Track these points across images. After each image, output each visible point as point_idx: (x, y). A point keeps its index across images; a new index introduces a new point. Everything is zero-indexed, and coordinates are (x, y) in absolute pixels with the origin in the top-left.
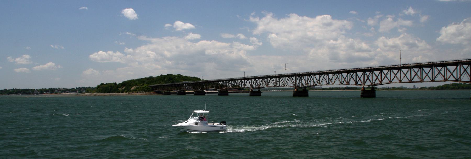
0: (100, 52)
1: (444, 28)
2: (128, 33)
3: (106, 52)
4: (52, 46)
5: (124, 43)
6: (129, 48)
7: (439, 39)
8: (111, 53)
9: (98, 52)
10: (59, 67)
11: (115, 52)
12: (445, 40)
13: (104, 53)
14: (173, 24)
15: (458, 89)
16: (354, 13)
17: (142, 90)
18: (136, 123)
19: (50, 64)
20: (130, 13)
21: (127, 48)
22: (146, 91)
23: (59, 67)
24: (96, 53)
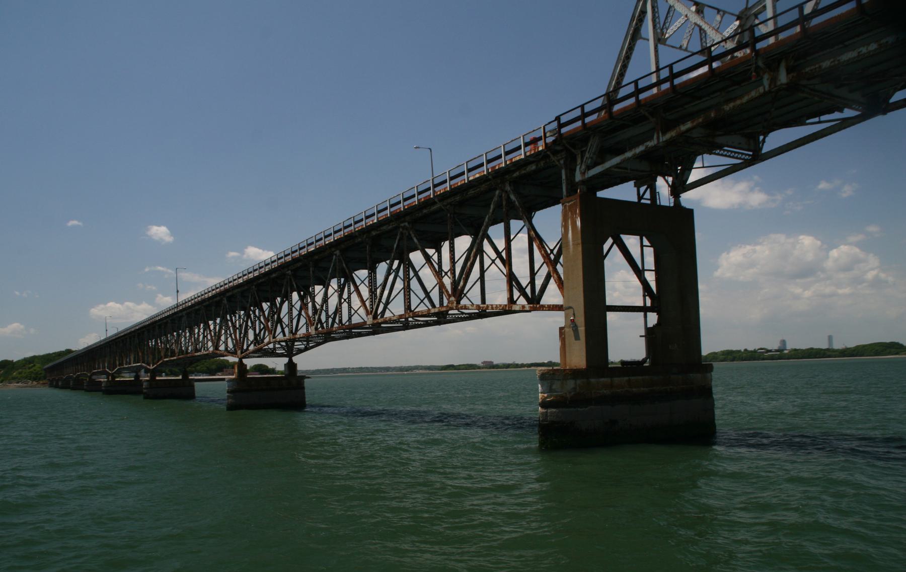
0: (111, 304)
1: (724, 255)
2: (160, 268)
3: (122, 304)
4: (17, 293)
5: (154, 288)
6: (166, 296)
7: (718, 273)
8: (130, 304)
9: (105, 303)
10: (32, 331)
11: (139, 303)
12: (728, 275)
13: (118, 305)
14: (243, 253)
15: (733, 360)
16: (579, 223)
17: (26, 378)
18: (76, 557)
19: (15, 325)
20: (160, 232)
21: (160, 296)
22: (35, 379)
23: (32, 331)
24: (102, 306)
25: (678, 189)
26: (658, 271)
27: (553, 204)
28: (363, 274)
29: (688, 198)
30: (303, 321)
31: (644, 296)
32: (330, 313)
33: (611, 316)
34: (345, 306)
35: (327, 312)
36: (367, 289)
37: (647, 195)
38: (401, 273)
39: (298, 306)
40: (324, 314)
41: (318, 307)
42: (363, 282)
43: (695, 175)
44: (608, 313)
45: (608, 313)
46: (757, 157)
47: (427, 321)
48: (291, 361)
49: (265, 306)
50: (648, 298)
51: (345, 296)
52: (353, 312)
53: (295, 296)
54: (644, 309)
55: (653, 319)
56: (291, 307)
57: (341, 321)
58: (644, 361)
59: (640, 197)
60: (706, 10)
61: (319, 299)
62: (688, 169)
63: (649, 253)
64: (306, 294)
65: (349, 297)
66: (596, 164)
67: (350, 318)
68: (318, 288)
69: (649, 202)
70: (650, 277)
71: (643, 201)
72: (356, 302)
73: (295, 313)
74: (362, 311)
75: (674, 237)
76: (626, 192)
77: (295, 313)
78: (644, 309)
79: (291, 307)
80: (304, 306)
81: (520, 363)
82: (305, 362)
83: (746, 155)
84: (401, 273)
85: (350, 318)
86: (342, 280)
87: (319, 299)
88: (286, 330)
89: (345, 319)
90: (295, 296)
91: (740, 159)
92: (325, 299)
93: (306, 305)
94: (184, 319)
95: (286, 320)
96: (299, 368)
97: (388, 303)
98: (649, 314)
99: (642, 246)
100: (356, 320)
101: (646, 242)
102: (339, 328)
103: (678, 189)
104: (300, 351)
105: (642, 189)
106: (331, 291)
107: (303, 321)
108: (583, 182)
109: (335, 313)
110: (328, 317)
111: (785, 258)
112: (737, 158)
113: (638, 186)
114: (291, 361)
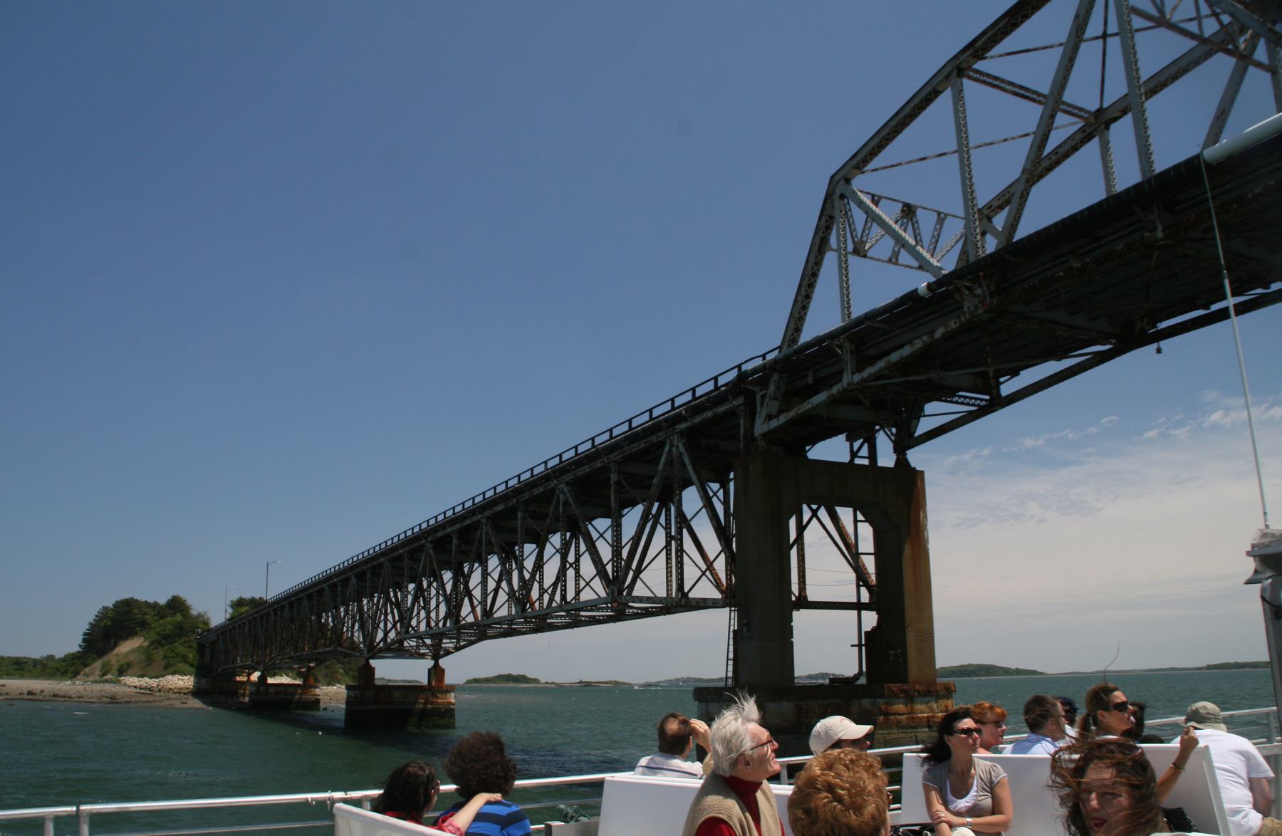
25: (901, 447)
26: (878, 554)
27: (836, 435)
28: (602, 524)
29: (916, 457)
30: (502, 596)
31: (858, 586)
32: (546, 586)
33: (801, 619)
34: (571, 573)
35: (541, 583)
36: (609, 550)
37: (865, 451)
38: (662, 520)
39: (496, 575)
40: (536, 586)
41: (527, 576)
42: (601, 535)
43: (924, 426)
44: (795, 613)
45: (795, 613)
46: (998, 403)
47: (593, 617)
48: (436, 665)
49: (447, 576)
50: (864, 591)
51: (571, 558)
52: (582, 584)
53: (493, 562)
54: (858, 606)
55: (870, 619)
56: (485, 575)
57: (563, 597)
58: (857, 677)
59: (854, 455)
60: (919, 212)
61: (529, 564)
62: (918, 414)
63: (866, 531)
64: (510, 555)
65: (577, 560)
66: (780, 412)
67: (578, 592)
68: (529, 548)
69: (866, 462)
70: (869, 563)
71: (857, 461)
72: (587, 568)
73: (491, 585)
74: (597, 584)
75: (896, 507)
76: (833, 450)
77: (491, 585)
78: (858, 606)
79: (485, 575)
80: (505, 575)
81: (1013, 667)
82: (463, 666)
83: (981, 400)
84: (662, 520)
85: (578, 592)
86: (568, 534)
87: (529, 564)
88: (478, 609)
89: (570, 595)
90: (493, 562)
91: (973, 405)
92: (539, 565)
93: (510, 574)
94: (305, 602)
95: (477, 593)
96: (377, 675)
97: (638, 571)
98: (864, 613)
99: (856, 521)
100: (587, 595)
101: (860, 517)
102: (560, 608)
103: (904, 443)
104: (448, 653)
105: (856, 445)
106: (549, 550)
107: (502, 596)
108: (764, 435)
109: (555, 585)
110: (542, 591)
111: (1065, 536)
112: (968, 404)
113: (851, 439)
114: (436, 665)
